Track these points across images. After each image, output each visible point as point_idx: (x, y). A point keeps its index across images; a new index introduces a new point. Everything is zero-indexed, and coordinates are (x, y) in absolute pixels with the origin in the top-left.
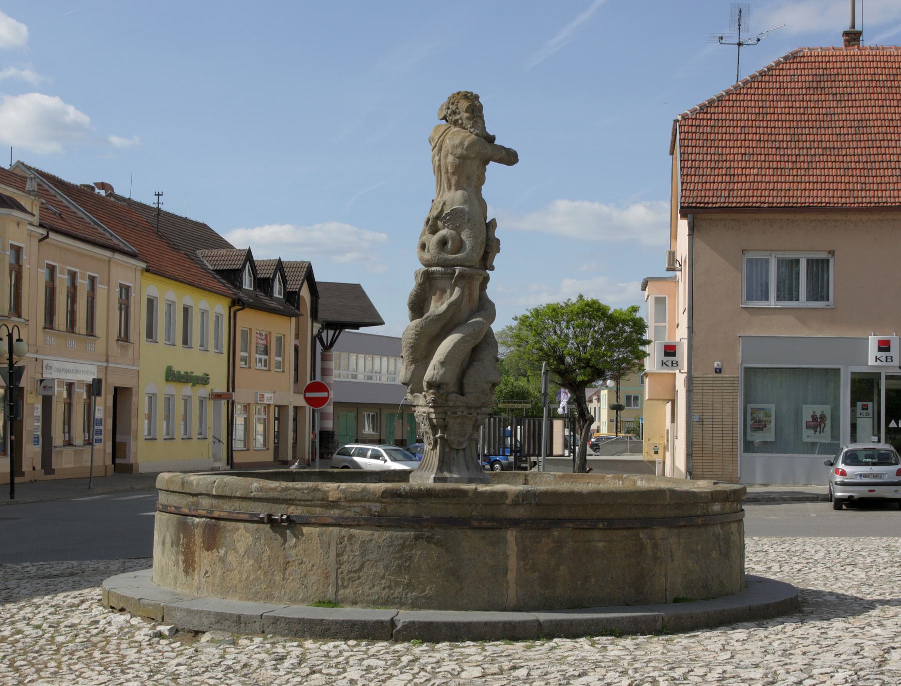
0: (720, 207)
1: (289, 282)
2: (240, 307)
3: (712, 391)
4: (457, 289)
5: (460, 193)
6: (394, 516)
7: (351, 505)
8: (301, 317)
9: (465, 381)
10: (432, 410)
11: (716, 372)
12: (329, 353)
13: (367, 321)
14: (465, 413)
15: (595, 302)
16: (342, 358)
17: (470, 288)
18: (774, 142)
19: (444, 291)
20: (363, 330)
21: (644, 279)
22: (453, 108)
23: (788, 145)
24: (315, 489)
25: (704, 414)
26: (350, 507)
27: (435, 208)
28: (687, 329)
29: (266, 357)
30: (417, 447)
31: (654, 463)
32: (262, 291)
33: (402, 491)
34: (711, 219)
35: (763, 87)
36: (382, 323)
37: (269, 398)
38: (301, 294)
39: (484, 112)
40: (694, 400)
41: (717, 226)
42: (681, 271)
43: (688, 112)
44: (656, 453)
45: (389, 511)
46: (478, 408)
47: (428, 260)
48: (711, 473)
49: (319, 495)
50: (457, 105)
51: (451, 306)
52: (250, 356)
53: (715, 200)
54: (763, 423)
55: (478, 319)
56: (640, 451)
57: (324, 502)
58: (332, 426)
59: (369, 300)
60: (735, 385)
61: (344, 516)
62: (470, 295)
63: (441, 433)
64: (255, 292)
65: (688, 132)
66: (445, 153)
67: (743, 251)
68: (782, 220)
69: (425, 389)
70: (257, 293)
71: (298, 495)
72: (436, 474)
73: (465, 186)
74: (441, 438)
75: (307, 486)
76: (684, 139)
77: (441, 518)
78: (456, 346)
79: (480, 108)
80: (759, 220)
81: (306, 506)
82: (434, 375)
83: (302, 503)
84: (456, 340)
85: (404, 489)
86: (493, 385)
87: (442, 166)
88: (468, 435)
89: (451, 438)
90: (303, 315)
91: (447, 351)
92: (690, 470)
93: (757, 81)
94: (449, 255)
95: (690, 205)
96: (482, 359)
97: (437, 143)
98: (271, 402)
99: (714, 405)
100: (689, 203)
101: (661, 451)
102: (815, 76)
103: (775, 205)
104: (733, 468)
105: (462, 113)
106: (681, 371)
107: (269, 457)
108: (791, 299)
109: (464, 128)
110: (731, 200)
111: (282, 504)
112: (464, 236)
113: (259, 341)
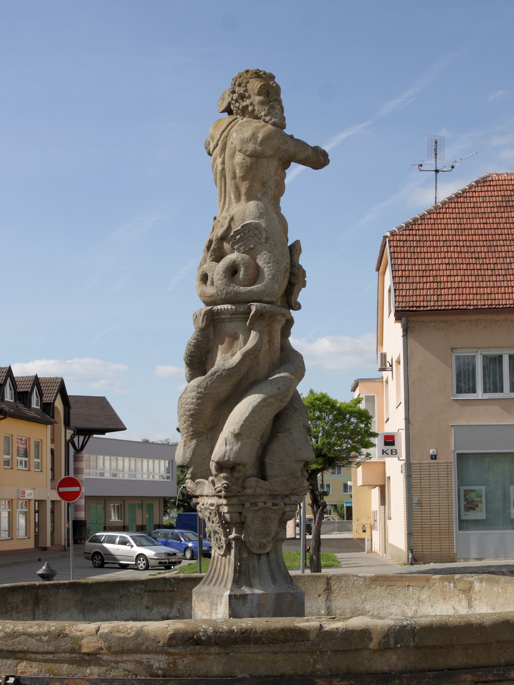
0: (430, 310)
1: (44, 395)
2: (3, 417)
3: (428, 476)
4: (253, 333)
5: (252, 204)
6: (190, 675)
7: (119, 659)
8: (55, 424)
9: (267, 460)
10: (224, 501)
11: (432, 459)
12: (80, 455)
13: (111, 427)
14: (269, 505)
15: (324, 396)
16: (91, 460)
17: (270, 333)
18: (473, 253)
19: (234, 338)
20: (108, 435)
21: (356, 381)
22: (241, 90)
23: (485, 255)
24: (60, 635)
25: (422, 497)
26: (117, 662)
27: (219, 225)
28: (404, 421)
29: (26, 459)
30: (158, 533)
31: (363, 540)
32: (22, 403)
33: (201, 634)
34: (423, 321)
35: (459, 207)
36: (124, 429)
37: (30, 494)
38: (55, 405)
39: (282, 96)
40: (413, 484)
41: (428, 327)
42: (392, 371)
43: (396, 229)
44: (364, 531)
45: (180, 667)
46: (287, 496)
47: (212, 296)
48: (430, 550)
49: (66, 644)
50: (246, 86)
51: (245, 356)
52: (12, 458)
53: (425, 304)
54: (475, 503)
55: (282, 374)
56: (350, 530)
57: (74, 655)
58: (84, 517)
59: (113, 410)
60: (449, 470)
61: (108, 677)
62: (271, 342)
63: (236, 533)
64: (15, 403)
65: (397, 246)
66: (231, 151)
67: (452, 348)
68: (486, 320)
69: (214, 472)
70: (17, 404)
71: (33, 644)
72: (231, 590)
73: (259, 195)
74: (235, 539)
75: (46, 629)
76: (394, 252)
77: (266, 677)
78: (256, 411)
79: (277, 90)
80: (465, 321)
81: (45, 661)
82: (226, 452)
83: (39, 657)
84: (256, 403)
85: (205, 631)
86: (304, 465)
87: (227, 170)
88: (273, 534)
89: (250, 539)
90: (57, 423)
91: (244, 419)
92: (412, 548)
93: (454, 202)
94: (241, 288)
95: (404, 309)
96: (289, 429)
97: (219, 140)
98: (31, 497)
99: (431, 489)
100: (403, 307)
101: (368, 530)
102: (504, 197)
103: (479, 307)
104: (451, 544)
105: (252, 96)
106: (400, 459)
107: (30, 544)
108: (495, 391)
109: (257, 118)
110: (440, 303)
111: (8, 658)
112: (261, 261)
113: (20, 445)
